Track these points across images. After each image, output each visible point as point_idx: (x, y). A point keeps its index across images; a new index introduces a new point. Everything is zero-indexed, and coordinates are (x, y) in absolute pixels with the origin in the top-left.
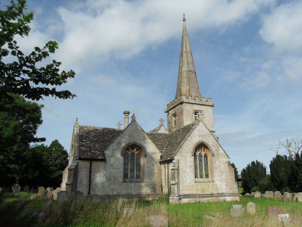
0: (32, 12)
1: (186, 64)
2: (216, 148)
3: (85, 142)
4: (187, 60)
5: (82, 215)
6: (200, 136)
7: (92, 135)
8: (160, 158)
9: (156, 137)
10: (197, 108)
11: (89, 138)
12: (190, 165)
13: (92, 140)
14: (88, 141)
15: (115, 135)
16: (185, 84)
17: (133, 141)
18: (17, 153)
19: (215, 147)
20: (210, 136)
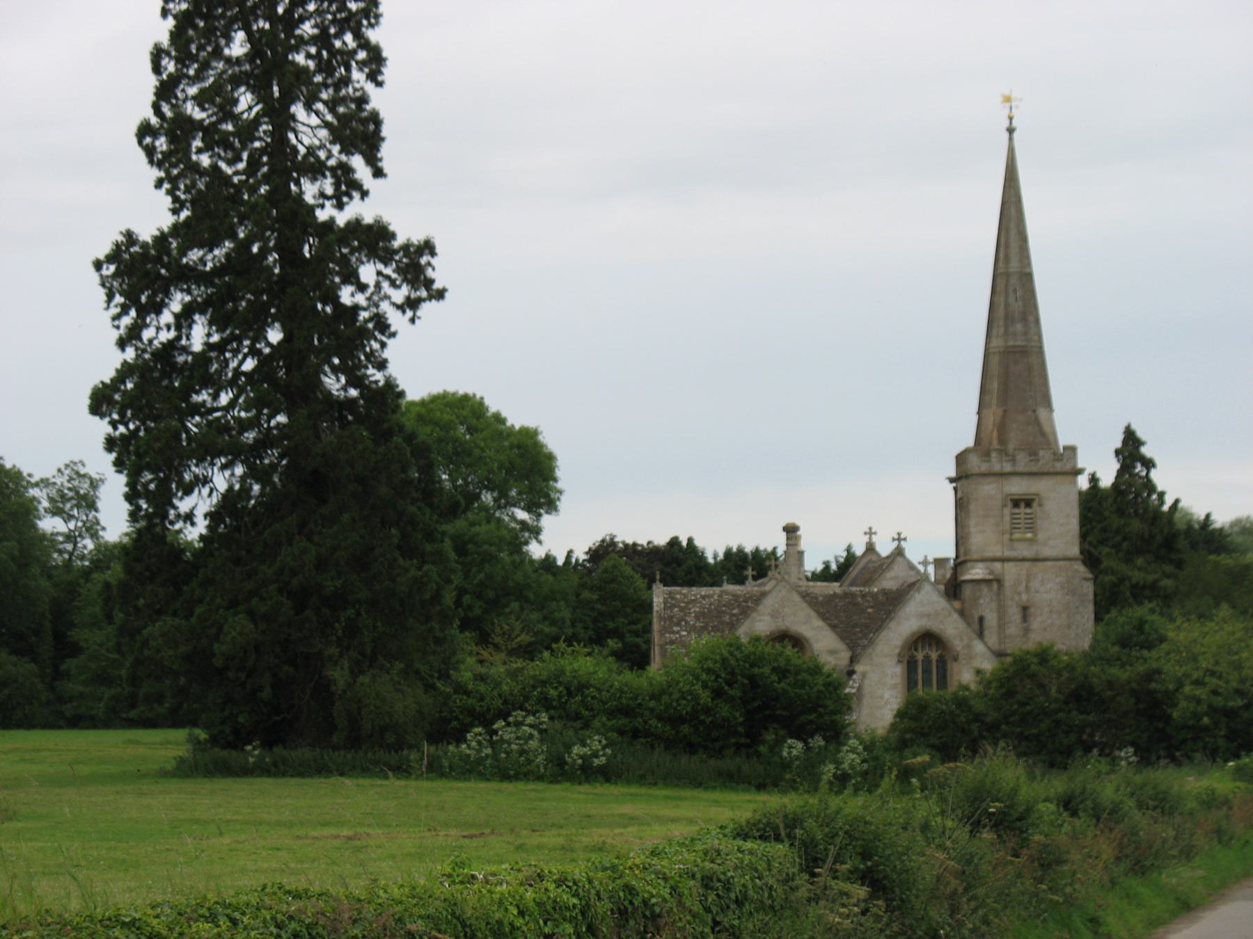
0: (549, 550)
1: (1001, 323)
2: (966, 642)
3: (678, 632)
4: (1007, 306)
5: (860, 824)
6: (921, 616)
7: (694, 612)
8: (965, 626)
9: (856, 604)
10: (1018, 487)
11: (687, 622)
12: (893, 682)
13: (694, 625)
14: (684, 630)
15: (748, 607)
16: (994, 401)
17: (782, 625)
18: (343, 256)
19: (962, 640)
20: (950, 615)
